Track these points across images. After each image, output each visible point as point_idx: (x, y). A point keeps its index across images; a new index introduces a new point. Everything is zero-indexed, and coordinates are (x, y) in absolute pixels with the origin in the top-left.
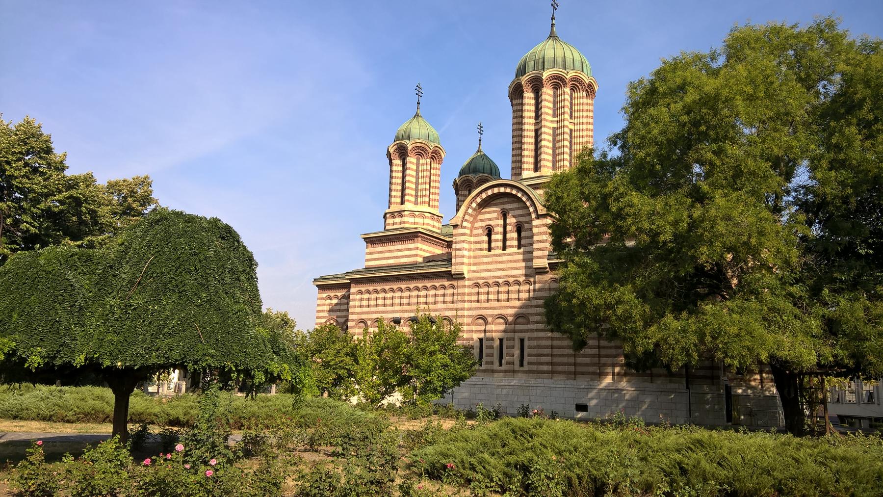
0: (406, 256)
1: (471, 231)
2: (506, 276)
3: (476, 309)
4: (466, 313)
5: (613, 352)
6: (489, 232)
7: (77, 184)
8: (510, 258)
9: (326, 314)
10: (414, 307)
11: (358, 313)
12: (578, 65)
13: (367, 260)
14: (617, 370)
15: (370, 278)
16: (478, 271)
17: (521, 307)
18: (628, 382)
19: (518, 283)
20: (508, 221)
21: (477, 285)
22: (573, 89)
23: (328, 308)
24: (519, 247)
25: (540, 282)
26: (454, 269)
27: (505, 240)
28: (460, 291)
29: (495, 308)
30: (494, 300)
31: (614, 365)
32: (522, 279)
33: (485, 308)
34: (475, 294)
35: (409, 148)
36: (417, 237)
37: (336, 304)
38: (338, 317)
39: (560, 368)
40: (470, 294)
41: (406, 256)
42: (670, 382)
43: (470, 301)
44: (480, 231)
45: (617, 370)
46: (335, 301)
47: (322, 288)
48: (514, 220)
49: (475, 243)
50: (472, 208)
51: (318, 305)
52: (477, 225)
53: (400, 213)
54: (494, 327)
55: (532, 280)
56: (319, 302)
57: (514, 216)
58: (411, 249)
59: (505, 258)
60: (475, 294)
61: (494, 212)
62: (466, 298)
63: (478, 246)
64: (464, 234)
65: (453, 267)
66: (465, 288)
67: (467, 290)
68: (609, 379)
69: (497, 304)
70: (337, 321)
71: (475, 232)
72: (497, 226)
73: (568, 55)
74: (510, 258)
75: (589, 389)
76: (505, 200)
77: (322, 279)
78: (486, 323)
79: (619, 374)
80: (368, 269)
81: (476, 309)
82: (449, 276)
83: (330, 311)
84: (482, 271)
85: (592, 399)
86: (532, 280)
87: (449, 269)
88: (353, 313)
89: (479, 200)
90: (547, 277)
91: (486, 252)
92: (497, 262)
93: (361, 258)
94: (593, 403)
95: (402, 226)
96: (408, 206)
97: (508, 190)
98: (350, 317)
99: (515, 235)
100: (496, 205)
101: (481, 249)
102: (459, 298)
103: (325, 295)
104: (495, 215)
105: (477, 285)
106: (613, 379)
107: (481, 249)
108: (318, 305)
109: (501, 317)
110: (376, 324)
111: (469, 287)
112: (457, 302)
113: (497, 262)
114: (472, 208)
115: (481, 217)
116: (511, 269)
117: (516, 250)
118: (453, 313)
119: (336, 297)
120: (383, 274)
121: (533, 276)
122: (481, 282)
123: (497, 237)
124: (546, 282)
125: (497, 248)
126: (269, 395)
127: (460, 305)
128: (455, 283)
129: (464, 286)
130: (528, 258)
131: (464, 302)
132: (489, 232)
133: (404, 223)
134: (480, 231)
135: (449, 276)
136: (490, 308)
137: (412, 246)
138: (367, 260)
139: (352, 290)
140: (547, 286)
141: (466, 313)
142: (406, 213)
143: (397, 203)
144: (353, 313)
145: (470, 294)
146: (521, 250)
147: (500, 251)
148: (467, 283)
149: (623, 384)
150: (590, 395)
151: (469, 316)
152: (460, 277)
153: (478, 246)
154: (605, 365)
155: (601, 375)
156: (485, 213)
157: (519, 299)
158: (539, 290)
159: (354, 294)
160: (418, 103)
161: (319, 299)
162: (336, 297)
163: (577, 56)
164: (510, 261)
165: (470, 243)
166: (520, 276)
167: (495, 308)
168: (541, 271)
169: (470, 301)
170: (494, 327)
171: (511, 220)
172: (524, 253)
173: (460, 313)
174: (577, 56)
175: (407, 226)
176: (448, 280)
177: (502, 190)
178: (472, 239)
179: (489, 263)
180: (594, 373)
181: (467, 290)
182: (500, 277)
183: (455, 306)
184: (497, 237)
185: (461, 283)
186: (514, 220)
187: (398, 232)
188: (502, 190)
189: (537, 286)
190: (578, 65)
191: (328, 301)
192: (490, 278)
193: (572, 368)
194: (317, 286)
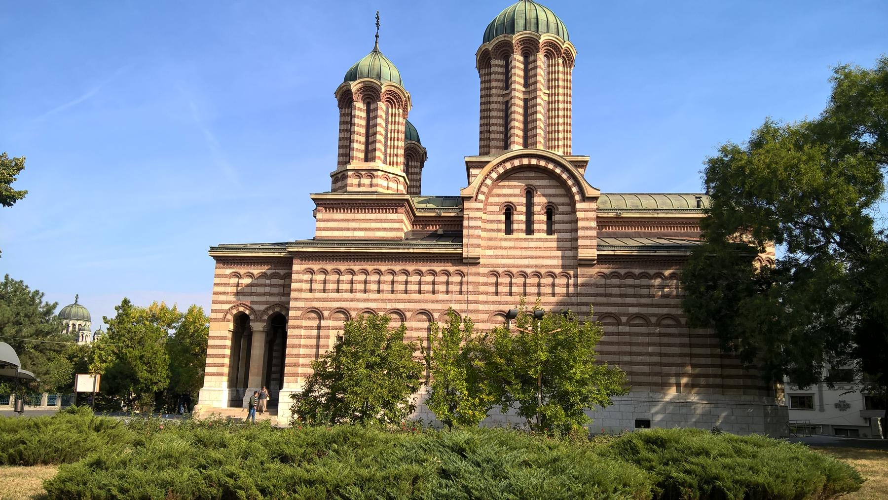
0: (384, 229)
1: (485, 207)
2: (536, 266)
3: (493, 303)
4: (481, 307)
5: (678, 360)
6: (509, 211)
7: (873, 87)
8: (540, 244)
9: (232, 298)
10: (517, 299)
11: (306, 300)
12: (553, 26)
13: (318, 229)
14: (684, 380)
15: (325, 253)
16: (496, 257)
17: (558, 304)
18: (698, 394)
19: (553, 275)
20: (536, 200)
21: (496, 274)
22: (549, 55)
23: (234, 289)
24: (550, 232)
25: (583, 276)
26: (466, 252)
27: (529, 223)
28: (472, 279)
29: (389, 301)
30: (388, 291)
31: (679, 375)
32: (557, 271)
33: (374, 301)
34: (306, 282)
35: (383, 90)
36: (403, 205)
37: (251, 285)
38: (252, 303)
39: (731, 382)
40: (485, 284)
41: (384, 229)
42: (744, 394)
43: (487, 294)
44: (497, 208)
45: (684, 380)
46: (247, 281)
47: (222, 261)
48: (544, 200)
49: (490, 222)
50: (491, 178)
51: (216, 285)
52: (492, 200)
53: (371, 173)
54: (331, 323)
55: (572, 273)
56: (218, 280)
57: (544, 195)
58: (392, 221)
59: (532, 244)
60: (306, 282)
61: (515, 187)
62: (482, 289)
63: (495, 226)
64: (478, 210)
65: (465, 249)
66: (476, 277)
67: (482, 279)
68: (672, 393)
69: (404, 296)
70: (251, 309)
71: (490, 208)
72: (520, 204)
73: (542, 16)
74: (540, 244)
75: (653, 402)
76: (532, 174)
77: (222, 248)
78: (321, 317)
79: (686, 385)
80: (315, 241)
81: (493, 303)
82: (458, 259)
83: (237, 294)
84: (502, 257)
85: (657, 413)
86: (572, 273)
87: (459, 251)
88: (296, 299)
89: (501, 170)
90: (594, 271)
91: (502, 235)
92: (521, 248)
93: (298, 225)
94: (658, 418)
95: (373, 189)
96: (378, 164)
97: (542, 163)
98: (292, 304)
99: (544, 218)
100: (518, 179)
101: (498, 231)
102: (471, 288)
103: (228, 271)
104: (517, 191)
105: (496, 274)
106: (678, 391)
107: (498, 231)
108: (216, 285)
109: (341, 311)
110: (447, 317)
111: (484, 275)
112: (468, 293)
113: (521, 248)
114: (491, 178)
115: (497, 191)
116: (543, 257)
117: (544, 235)
118: (464, 306)
119: (251, 275)
120: (352, 250)
121: (575, 267)
122: (500, 270)
123: (519, 217)
124: (591, 276)
125: (539, 231)
126: (38, 408)
127: (471, 297)
128: (464, 269)
129: (478, 274)
130: (570, 245)
131: (478, 293)
132: (509, 211)
133: (377, 185)
134: (497, 208)
135: (458, 259)
136: (381, 301)
137: (394, 216)
138: (318, 229)
139: (295, 267)
140: (593, 281)
141: (481, 307)
142: (380, 173)
143: (359, 159)
144: (296, 299)
145: (485, 284)
146: (555, 236)
147: (523, 235)
148: (482, 270)
149: (694, 398)
150: (654, 410)
151: (485, 312)
152: (474, 262)
153: (495, 226)
154: (669, 375)
155: (663, 386)
156: (504, 187)
157: (553, 295)
158: (583, 285)
159: (298, 272)
160: (377, 36)
161: (217, 276)
162: (251, 275)
163: (552, 18)
164: (539, 249)
165: (483, 221)
166: (555, 267)
167: (389, 301)
168: (587, 263)
169: (487, 294)
170: (331, 323)
171: (540, 200)
172: (558, 240)
173: (472, 307)
174: (552, 18)
175: (380, 190)
176: (454, 264)
177: (534, 162)
178: (485, 217)
179: (510, 248)
180: (656, 384)
181: (482, 279)
182: (528, 266)
183: (465, 297)
184: (519, 217)
185: (472, 269)
186: (544, 200)
187: (374, 197)
188: (534, 162)
189: (580, 280)
190: (553, 26)
191: (234, 281)
192: (513, 266)
193: (718, 381)
194: (214, 257)
